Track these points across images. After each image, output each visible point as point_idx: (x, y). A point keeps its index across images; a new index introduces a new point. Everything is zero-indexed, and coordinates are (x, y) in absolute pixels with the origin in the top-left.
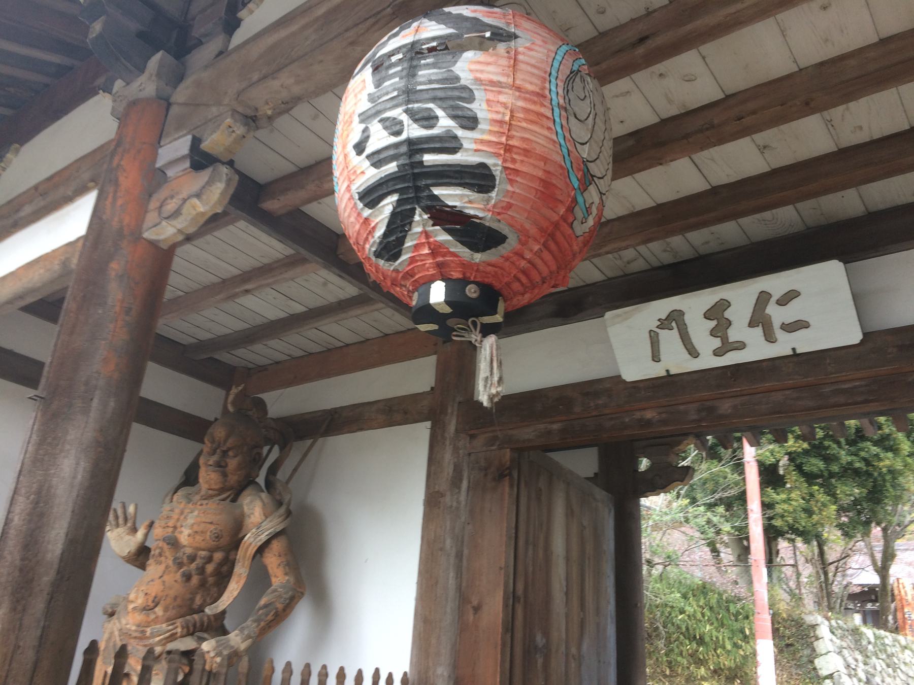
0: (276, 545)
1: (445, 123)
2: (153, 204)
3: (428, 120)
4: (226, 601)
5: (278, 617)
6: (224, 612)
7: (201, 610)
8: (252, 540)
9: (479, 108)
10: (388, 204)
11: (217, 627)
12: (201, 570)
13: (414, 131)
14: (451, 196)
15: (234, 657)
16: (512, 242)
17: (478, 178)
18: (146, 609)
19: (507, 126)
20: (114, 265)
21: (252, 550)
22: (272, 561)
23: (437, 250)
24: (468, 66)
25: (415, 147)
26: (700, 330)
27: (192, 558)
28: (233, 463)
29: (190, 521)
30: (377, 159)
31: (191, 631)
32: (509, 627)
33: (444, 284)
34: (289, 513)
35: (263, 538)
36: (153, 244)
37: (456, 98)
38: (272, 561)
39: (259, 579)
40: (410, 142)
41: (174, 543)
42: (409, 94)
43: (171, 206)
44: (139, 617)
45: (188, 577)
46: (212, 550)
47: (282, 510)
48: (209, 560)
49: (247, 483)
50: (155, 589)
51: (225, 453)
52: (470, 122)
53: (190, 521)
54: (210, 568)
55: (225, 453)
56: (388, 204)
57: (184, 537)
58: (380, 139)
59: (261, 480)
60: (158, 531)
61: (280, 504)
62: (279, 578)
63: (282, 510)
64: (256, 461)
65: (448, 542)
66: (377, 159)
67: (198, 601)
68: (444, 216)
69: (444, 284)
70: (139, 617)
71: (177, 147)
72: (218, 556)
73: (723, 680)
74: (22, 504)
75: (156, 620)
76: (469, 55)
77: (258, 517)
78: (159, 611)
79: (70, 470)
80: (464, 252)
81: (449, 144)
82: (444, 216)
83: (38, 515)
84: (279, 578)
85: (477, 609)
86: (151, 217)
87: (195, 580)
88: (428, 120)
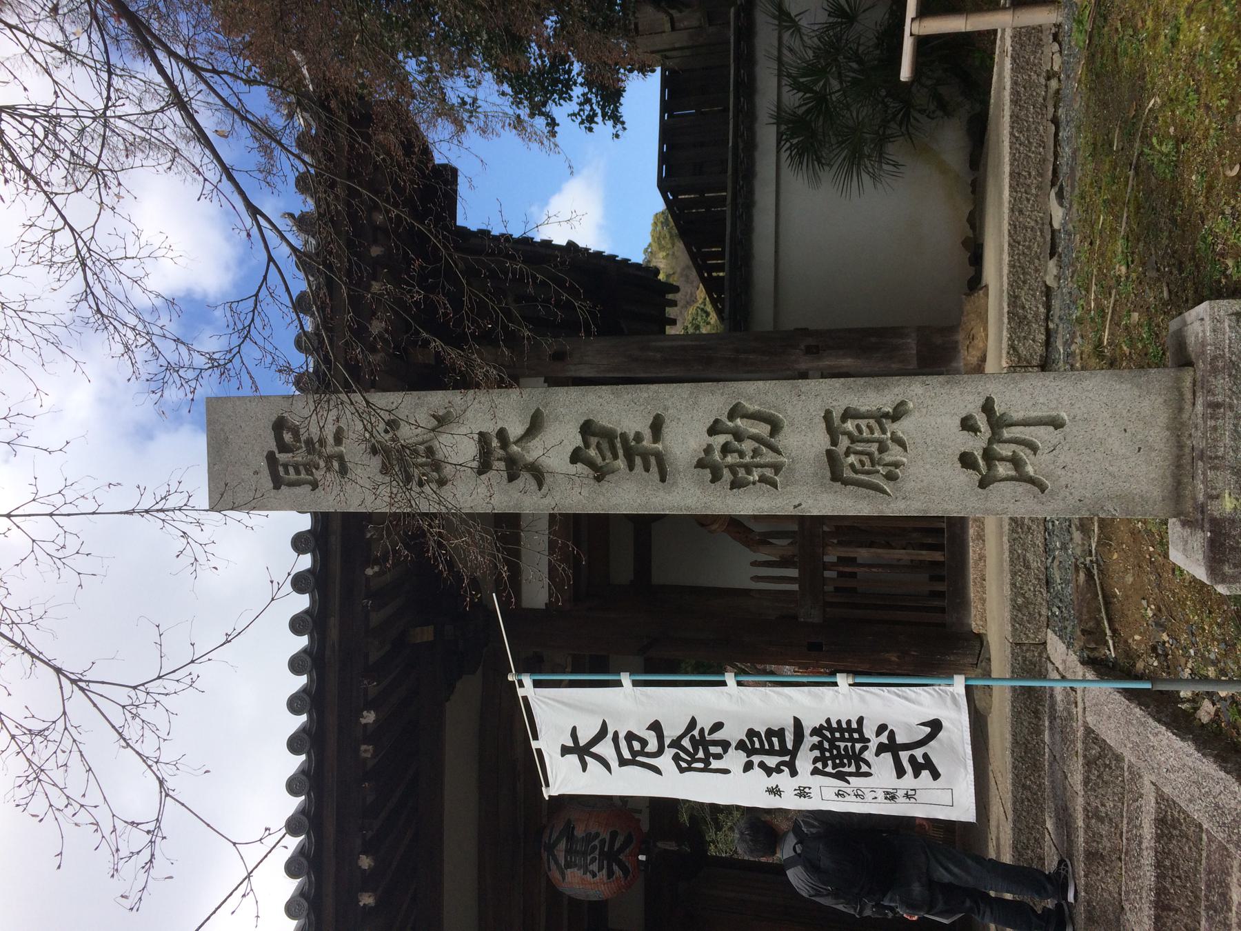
1: (596, 842)
3: (594, 848)
9: (593, 831)
10: (615, 868)
17: (614, 835)
24: (579, 833)
26: (804, 441)
30: (600, 869)
33: (460, 221)
37: (589, 838)
52: (597, 835)
56: (615, 868)
66: (600, 869)
68: (621, 850)
69: (460, 221)
73: (869, 732)
80: (632, 847)
81: (603, 842)
82: (621, 850)
88: (594, 848)
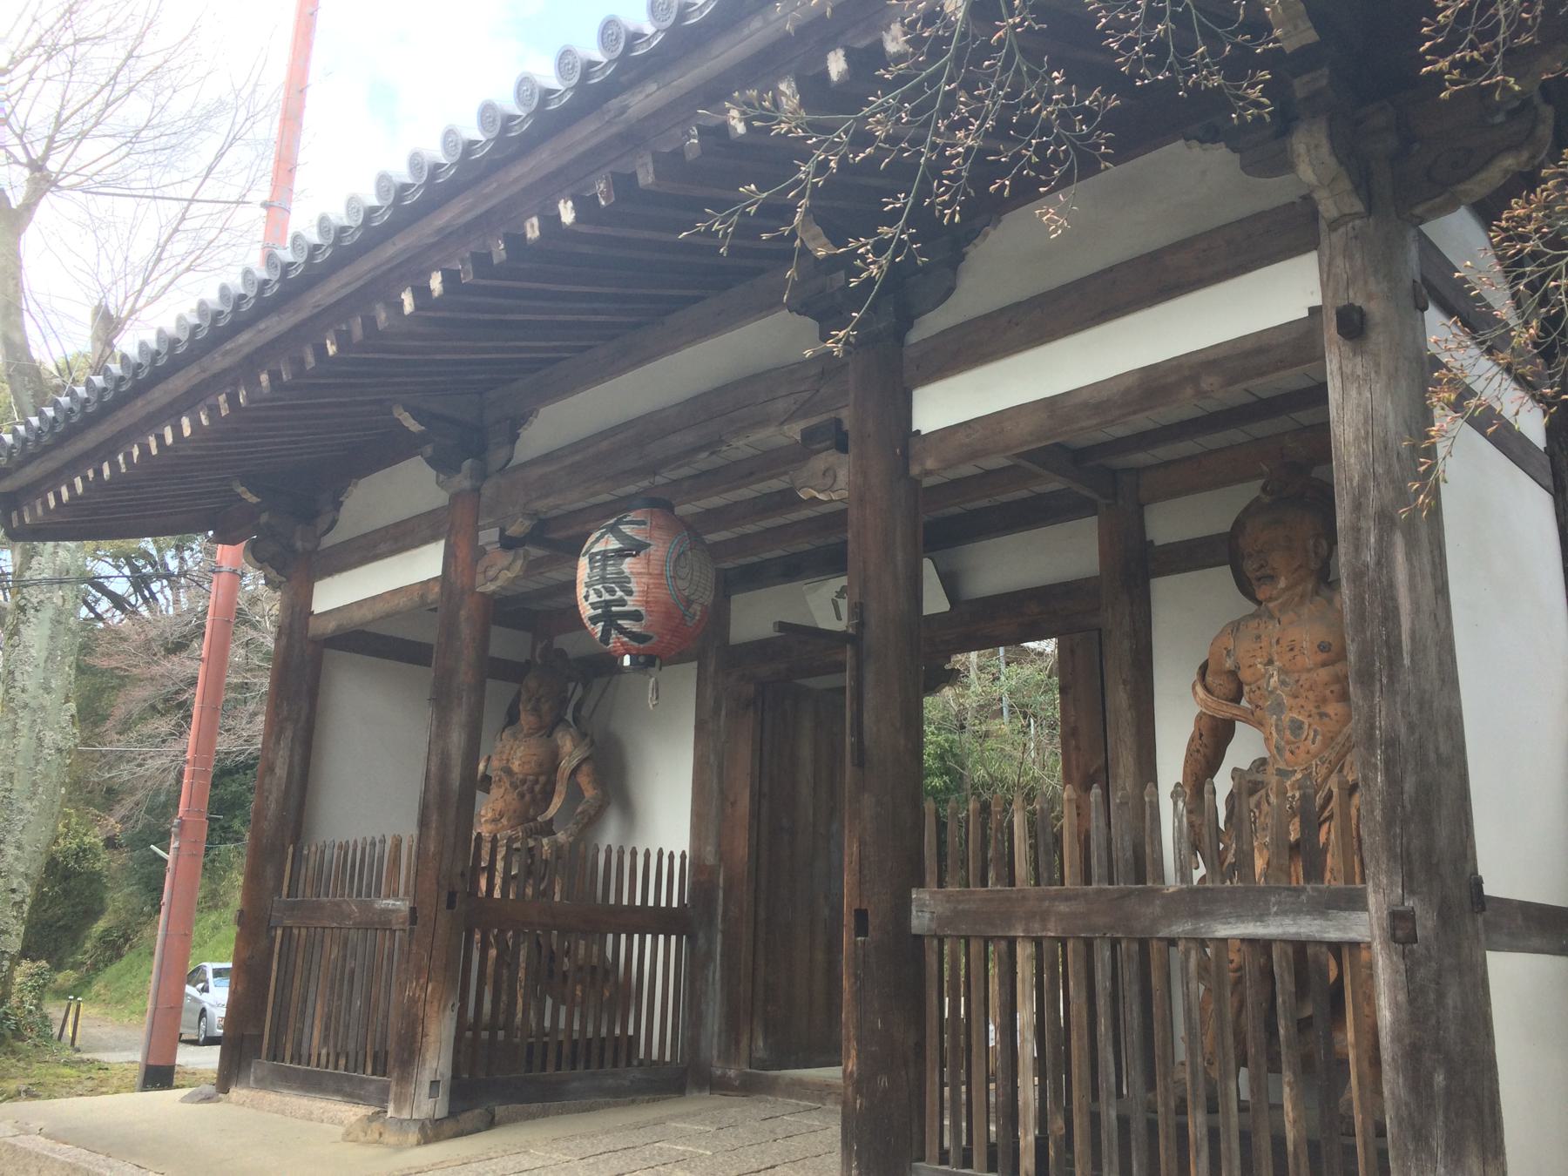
0: (585, 768)
1: (619, 593)
2: (480, 568)
4: (552, 810)
5: (593, 821)
6: (551, 820)
7: (534, 819)
8: (566, 765)
9: (633, 586)
11: (548, 829)
12: (531, 790)
13: (607, 597)
14: (625, 623)
15: (558, 849)
16: (656, 639)
17: (635, 616)
18: (494, 821)
19: (646, 593)
20: (463, 613)
21: (567, 772)
22: (584, 780)
23: (623, 644)
24: (628, 565)
25: (608, 604)
27: (524, 782)
28: (545, 707)
29: (519, 754)
31: (530, 833)
32: (755, 814)
34: (592, 743)
35: (575, 763)
36: (482, 594)
37: (622, 581)
38: (584, 780)
39: (575, 794)
40: (606, 602)
41: (508, 771)
42: (603, 580)
43: (491, 573)
44: (490, 827)
45: (522, 796)
46: (537, 775)
47: (588, 740)
48: (537, 782)
49: (559, 720)
50: (500, 805)
51: (538, 700)
52: (630, 593)
53: (519, 754)
54: (537, 788)
55: (538, 700)
57: (516, 766)
58: (593, 598)
59: (569, 717)
60: (495, 763)
61: (584, 735)
62: (590, 792)
63: (588, 740)
64: (564, 702)
65: (712, 757)
67: (531, 812)
70: (490, 827)
71: (489, 536)
72: (542, 779)
74: (434, 759)
75: (503, 828)
76: (628, 560)
77: (570, 751)
78: (504, 821)
79: (457, 739)
81: (622, 602)
82: (622, 630)
83: (445, 765)
84: (590, 792)
85: (733, 804)
86: (480, 578)
87: (528, 797)
88: (611, 591)
